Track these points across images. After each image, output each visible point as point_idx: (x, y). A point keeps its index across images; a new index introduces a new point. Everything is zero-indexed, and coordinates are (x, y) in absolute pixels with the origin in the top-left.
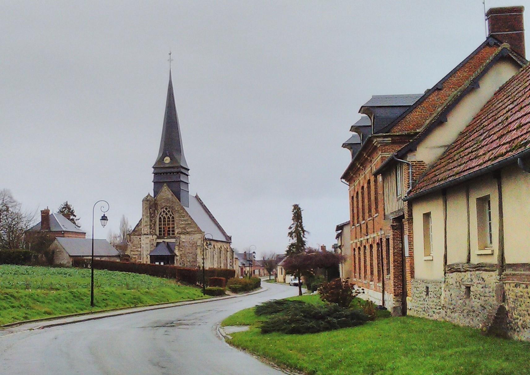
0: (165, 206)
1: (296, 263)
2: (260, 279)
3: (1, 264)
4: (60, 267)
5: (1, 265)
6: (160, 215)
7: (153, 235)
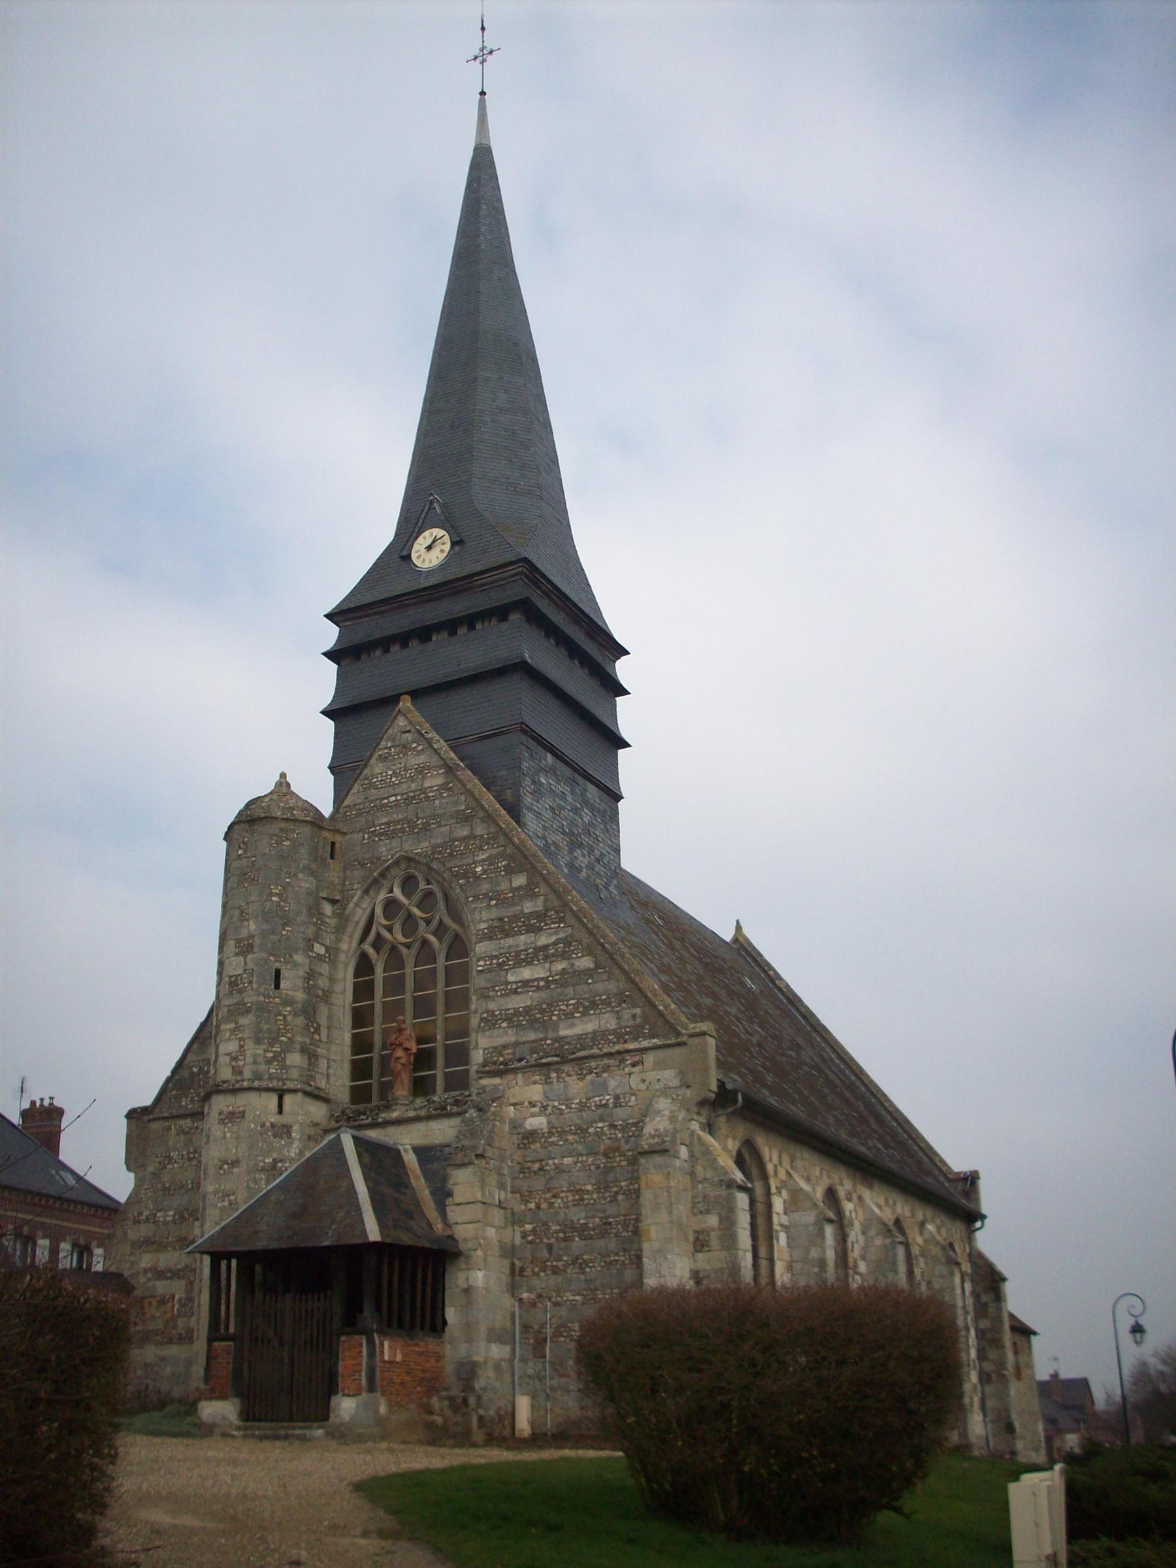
0: (397, 863)
1: (719, 1286)
2: (376, 1391)
3: (1010, 1563)
4: (797, 1267)
5: (1173, 1444)
6: (363, 939)
7: (574, 986)
